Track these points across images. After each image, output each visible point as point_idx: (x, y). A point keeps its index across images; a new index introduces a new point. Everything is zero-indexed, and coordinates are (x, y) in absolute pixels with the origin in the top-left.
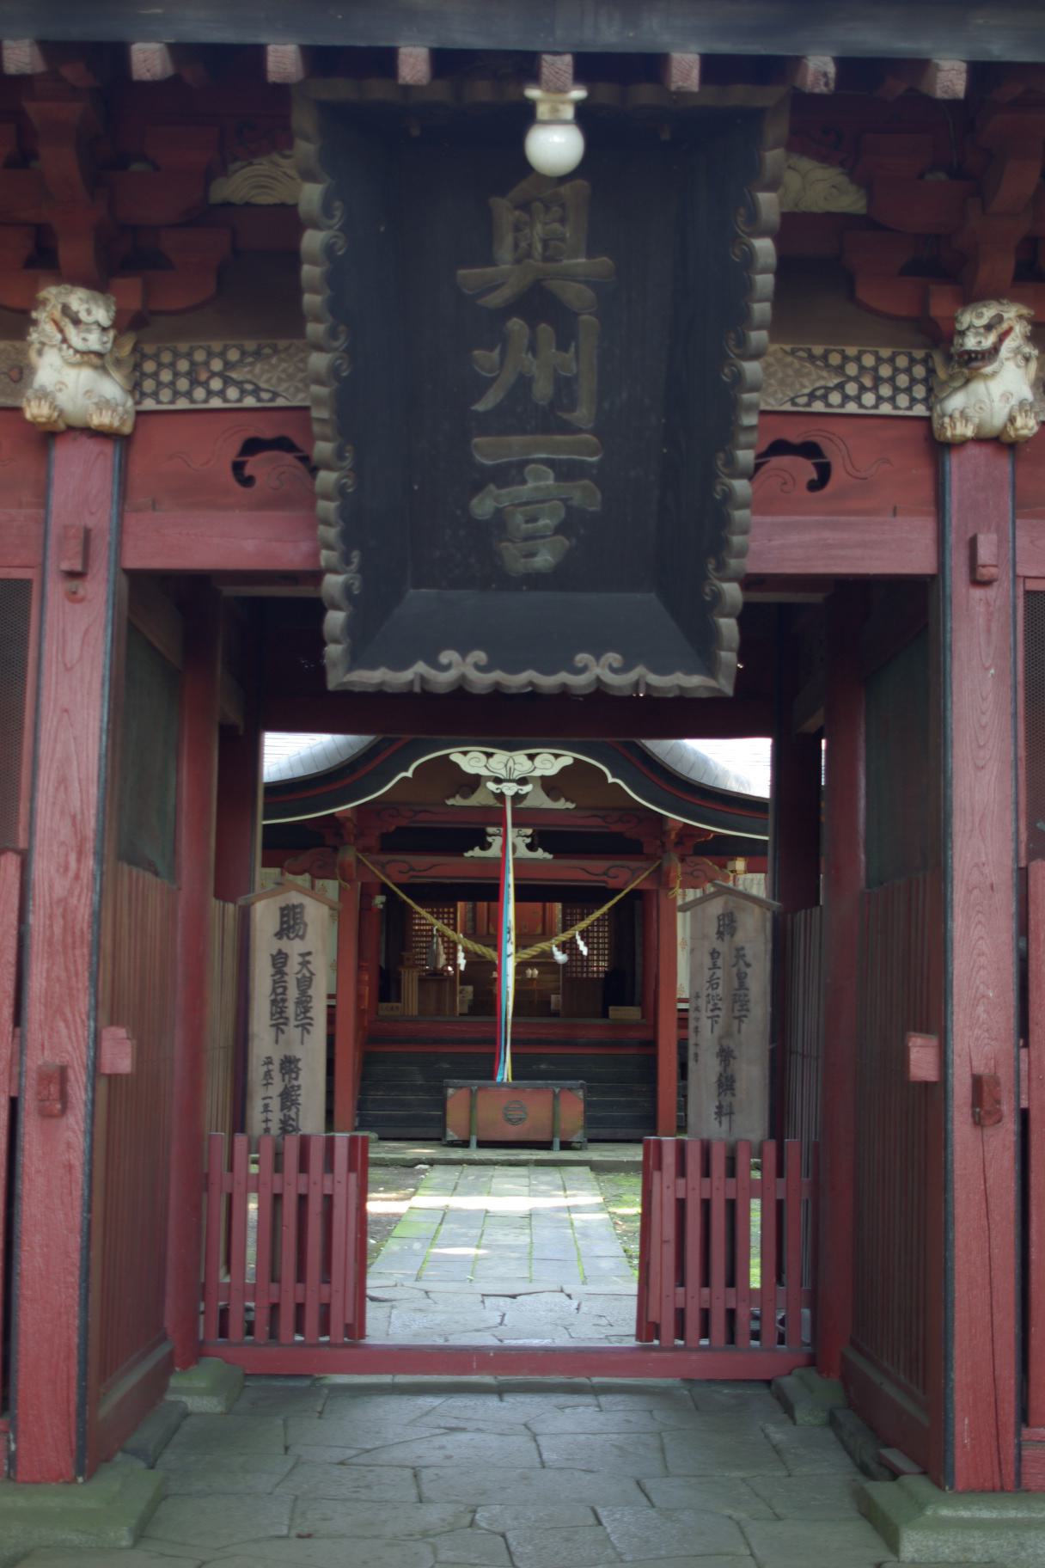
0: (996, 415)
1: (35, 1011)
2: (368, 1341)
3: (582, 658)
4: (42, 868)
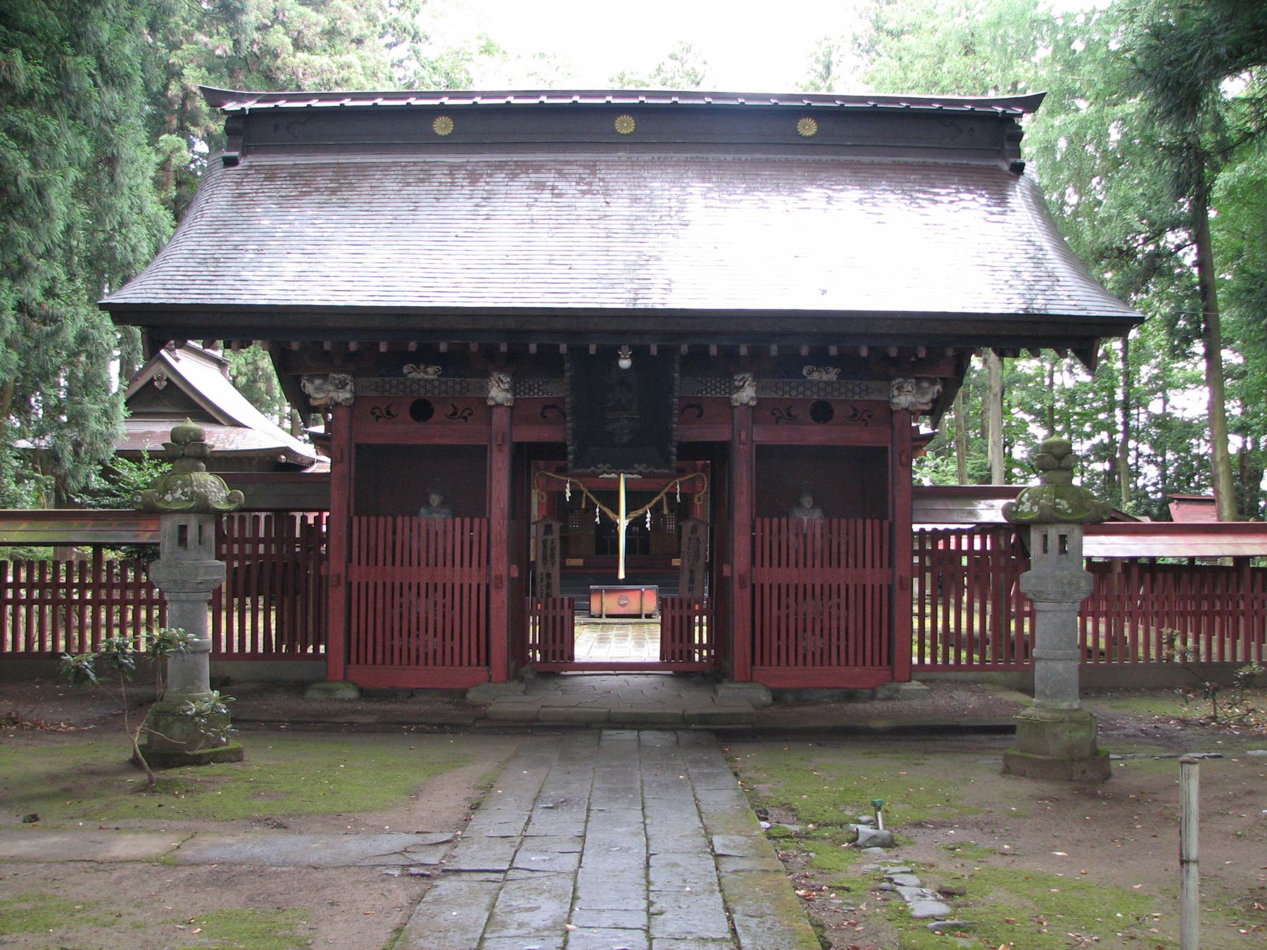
0: (745, 400)
1: (493, 560)
2: (576, 661)
3: (636, 465)
4: (493, 522)
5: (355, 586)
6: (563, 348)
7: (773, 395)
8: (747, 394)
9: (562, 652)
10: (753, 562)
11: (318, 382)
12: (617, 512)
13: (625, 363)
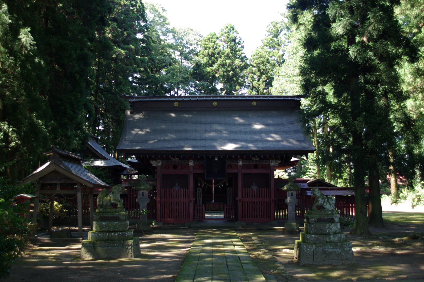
1: (190, 197)
5: (162, 202)
6: (205, 157)
7: (246, 163)
8: (241, 163)
9: (203, 217)
10: (242, 197)
11: (154, 161)
12: (212, 185)
13: (216, 159)
